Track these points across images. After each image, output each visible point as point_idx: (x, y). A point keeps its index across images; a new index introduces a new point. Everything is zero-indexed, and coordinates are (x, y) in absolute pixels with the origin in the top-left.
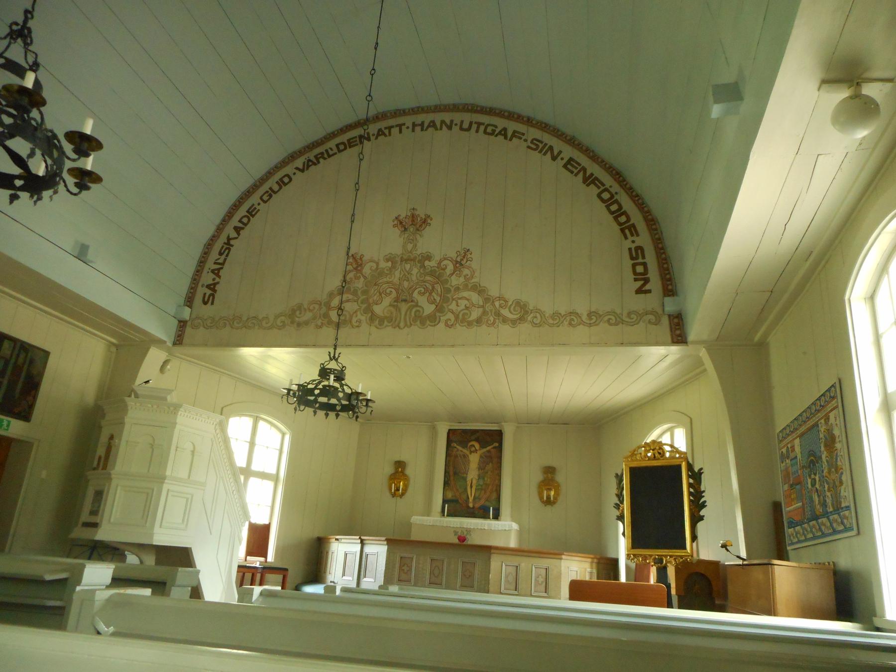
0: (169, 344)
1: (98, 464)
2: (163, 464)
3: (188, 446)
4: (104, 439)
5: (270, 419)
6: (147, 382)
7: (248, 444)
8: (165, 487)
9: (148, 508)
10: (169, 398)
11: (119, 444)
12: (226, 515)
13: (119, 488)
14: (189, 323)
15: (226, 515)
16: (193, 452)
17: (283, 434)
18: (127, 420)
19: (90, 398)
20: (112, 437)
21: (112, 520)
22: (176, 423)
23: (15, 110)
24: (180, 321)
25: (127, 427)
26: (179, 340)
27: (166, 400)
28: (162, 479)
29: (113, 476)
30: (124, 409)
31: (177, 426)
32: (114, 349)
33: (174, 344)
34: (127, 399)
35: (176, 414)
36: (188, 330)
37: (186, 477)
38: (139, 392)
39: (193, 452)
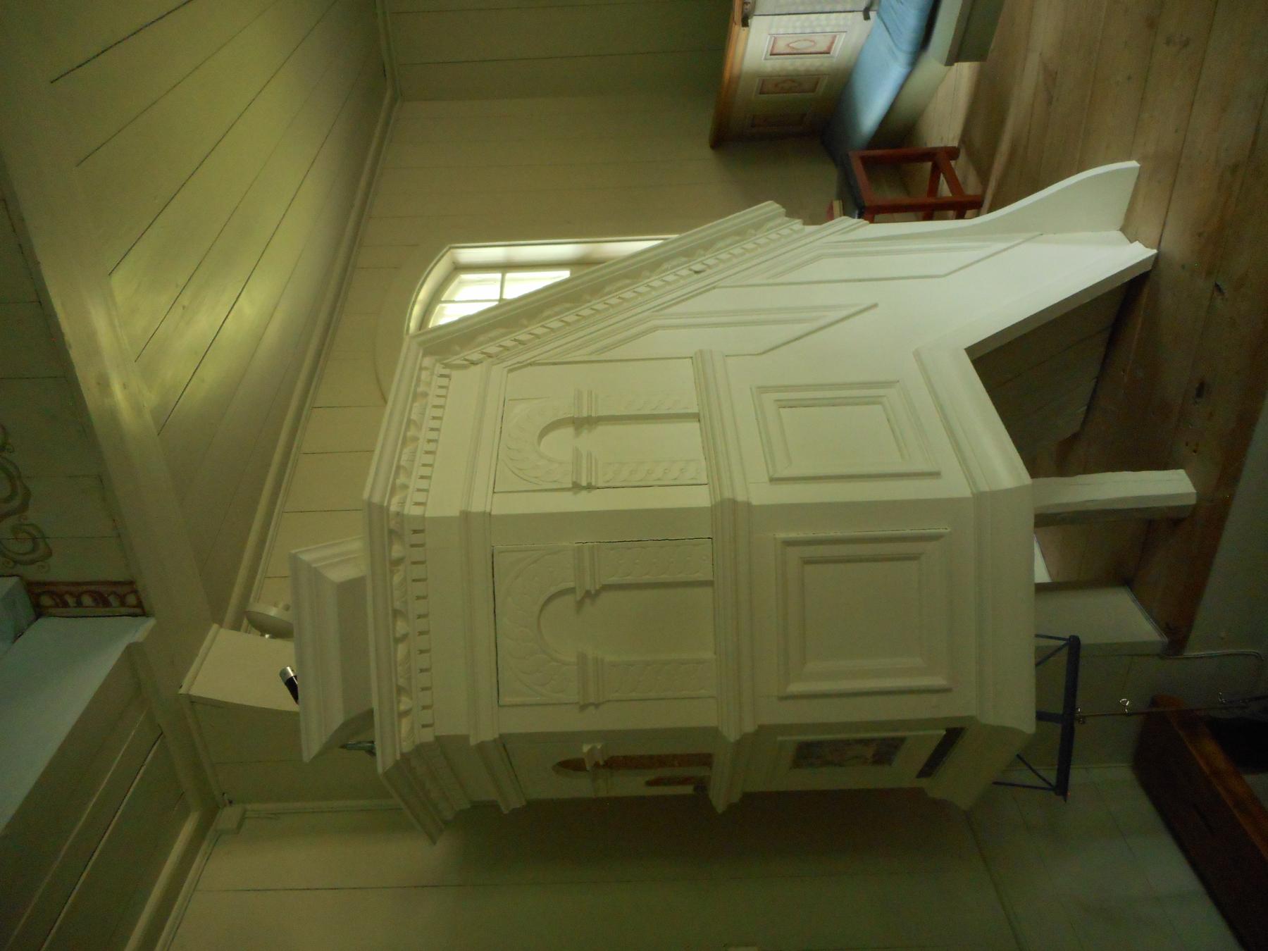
0: (140, 630)
1: (685, 781)
2: (663, 527)
3: (561, 443)
4: (580, 787)
5: (423, 294)
6: (291, 684)
7: (509, 276)
8: (760, 493)
9: (867, 549)
10: (338, 575)
11: (604, 735)
12: (792, 277)
13: (795, 688)
14: (33, 573)
15: (792, 277)
16: (581, 423)
17: (459, 268)
18: (487, 733)
19: (416, 854)
20: (573, 766)
21: (939, 681)
22: (466, 516)
23: (1129, 159)
24: (39, 612)
25: (514, 724)
26: (118, 597)
27: (351, 590)
28: (731, 516)
29: (749, 728)
30: (444, 751)
31: (478, 505)
32: (228, 817)
33: (141, 611)
34: (385, 760)
35: (420, 528)
36: (59, 570)
37: (693, 426)
38: (338, 719)
39: (581, 423)
